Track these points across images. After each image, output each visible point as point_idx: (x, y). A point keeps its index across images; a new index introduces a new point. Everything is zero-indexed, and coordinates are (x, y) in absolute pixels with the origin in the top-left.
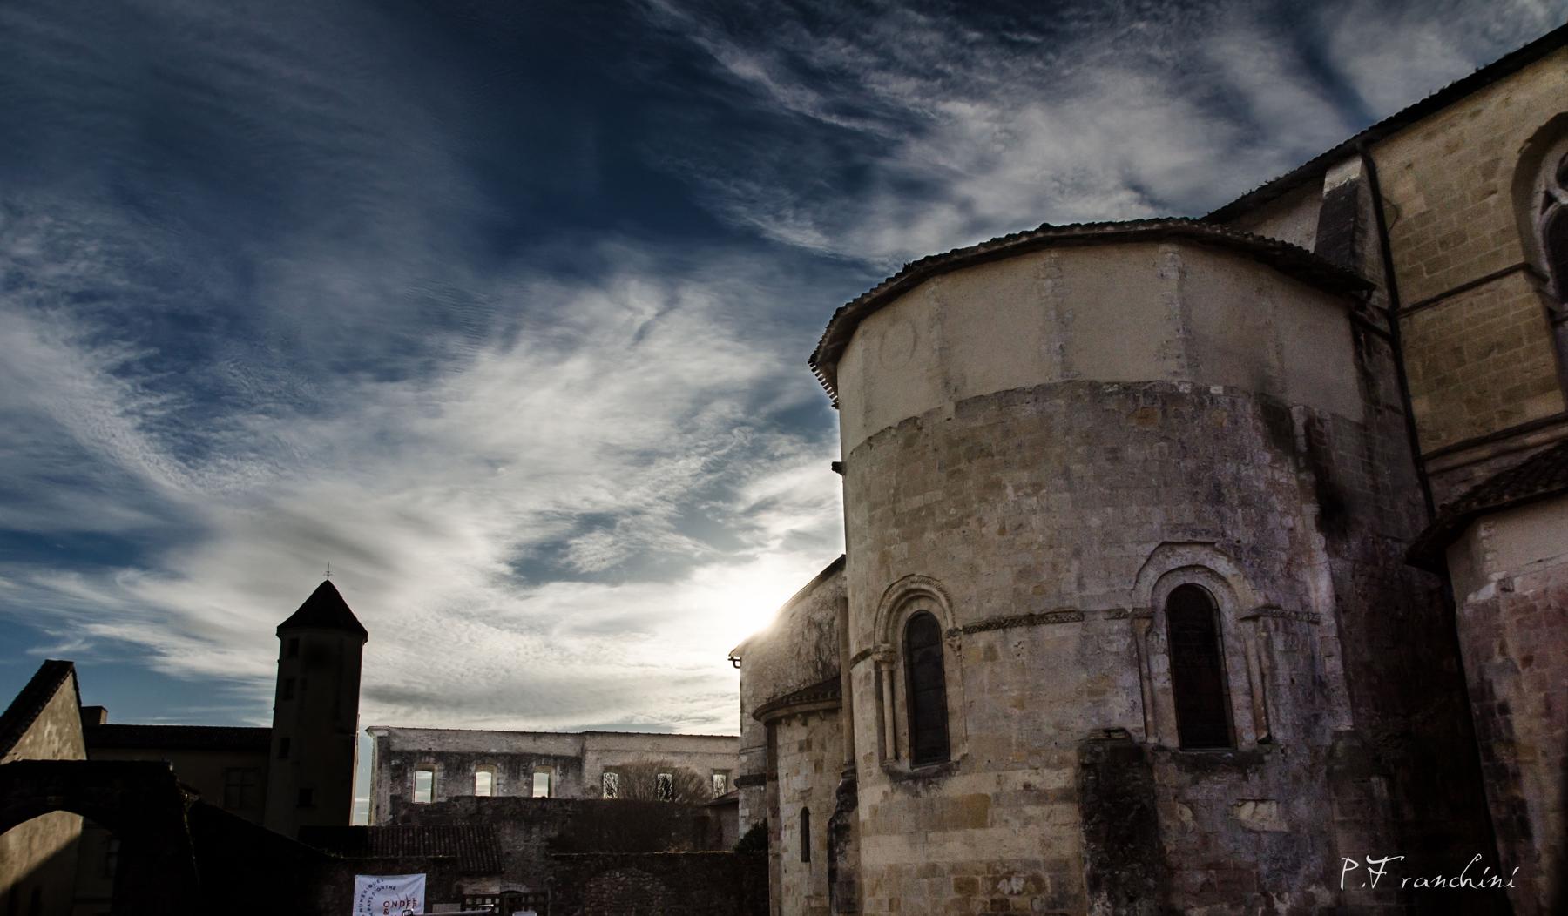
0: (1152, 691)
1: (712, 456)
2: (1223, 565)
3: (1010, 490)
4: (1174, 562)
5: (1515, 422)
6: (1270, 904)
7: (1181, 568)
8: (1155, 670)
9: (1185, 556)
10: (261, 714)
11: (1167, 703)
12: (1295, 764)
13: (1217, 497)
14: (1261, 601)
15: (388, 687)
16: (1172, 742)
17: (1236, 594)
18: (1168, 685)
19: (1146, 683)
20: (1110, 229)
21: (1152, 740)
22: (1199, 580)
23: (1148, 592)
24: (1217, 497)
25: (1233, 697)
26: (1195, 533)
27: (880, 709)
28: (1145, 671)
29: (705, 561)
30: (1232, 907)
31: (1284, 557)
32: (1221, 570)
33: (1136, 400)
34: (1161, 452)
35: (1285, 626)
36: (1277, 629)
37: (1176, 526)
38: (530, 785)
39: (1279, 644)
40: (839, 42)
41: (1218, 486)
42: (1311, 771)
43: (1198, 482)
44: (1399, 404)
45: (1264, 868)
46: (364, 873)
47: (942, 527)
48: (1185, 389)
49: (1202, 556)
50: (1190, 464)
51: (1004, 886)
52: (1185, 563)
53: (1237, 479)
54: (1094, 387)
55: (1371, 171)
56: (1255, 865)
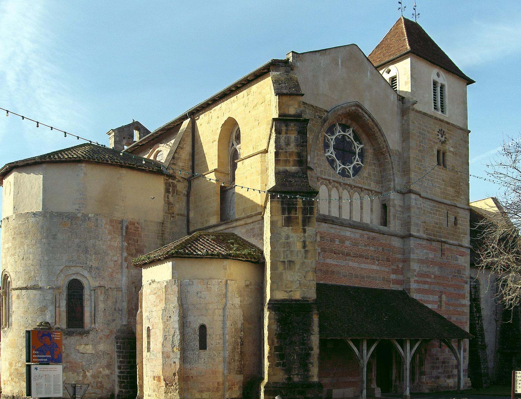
0: (60, 311)
1: (425, 269)
2: (86, 273)
3: (25, 246)
4: (70, 272)
5: (208, 225)
6: (85, 373)
7: (73, 274)
8: (61, 305)
9: (74, 270)
10: (59, 393)
11: (64, 315)
12: (101, 334)
13: (86, 251)
14: (97, 284)
15: (146, 174)
16: (64, 326)
17: (89, 282)
18: (65, 309)
19: (57, 309)
20: (160, 133)
21: (57, 326)
22: (79, 278)
23: (63, 282)
24: (86, 251)
25: (85, 314)
26: (434, 235)
27: (9, 301)
28: (58, 305)
29: (318, 210)
30: (73, 373)
31: (110, 270)
32: (85, 275)
33: (63, 219)
34: (69, 237)
35: (105, 292)
36: (101, 293)
37: (70, 261)
38: (476, 274)
39: (101, 298)
40: (450, 385)
41: (86, 248)
42: (107, 336)
43: (80, 247)
44: (186, 213)
45: (84, 363)
46: (43, 177)
47: (384, 154)
48: (79, 215)
49: (79, 270)
50: (77, 241)
51: (281, 151)
52: (73, 272)
53: (94, 246)
54: (51, 213)
55: (193, 125)
56: (81, 362)
